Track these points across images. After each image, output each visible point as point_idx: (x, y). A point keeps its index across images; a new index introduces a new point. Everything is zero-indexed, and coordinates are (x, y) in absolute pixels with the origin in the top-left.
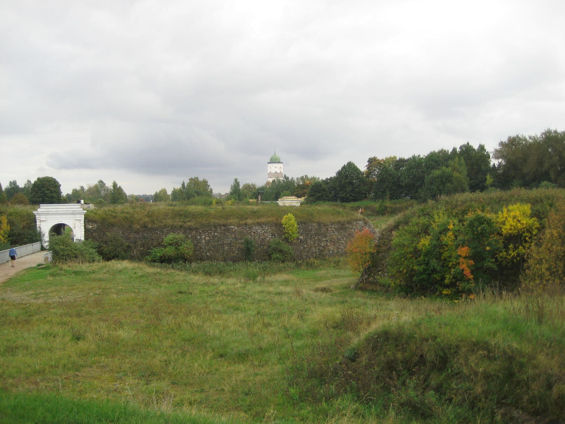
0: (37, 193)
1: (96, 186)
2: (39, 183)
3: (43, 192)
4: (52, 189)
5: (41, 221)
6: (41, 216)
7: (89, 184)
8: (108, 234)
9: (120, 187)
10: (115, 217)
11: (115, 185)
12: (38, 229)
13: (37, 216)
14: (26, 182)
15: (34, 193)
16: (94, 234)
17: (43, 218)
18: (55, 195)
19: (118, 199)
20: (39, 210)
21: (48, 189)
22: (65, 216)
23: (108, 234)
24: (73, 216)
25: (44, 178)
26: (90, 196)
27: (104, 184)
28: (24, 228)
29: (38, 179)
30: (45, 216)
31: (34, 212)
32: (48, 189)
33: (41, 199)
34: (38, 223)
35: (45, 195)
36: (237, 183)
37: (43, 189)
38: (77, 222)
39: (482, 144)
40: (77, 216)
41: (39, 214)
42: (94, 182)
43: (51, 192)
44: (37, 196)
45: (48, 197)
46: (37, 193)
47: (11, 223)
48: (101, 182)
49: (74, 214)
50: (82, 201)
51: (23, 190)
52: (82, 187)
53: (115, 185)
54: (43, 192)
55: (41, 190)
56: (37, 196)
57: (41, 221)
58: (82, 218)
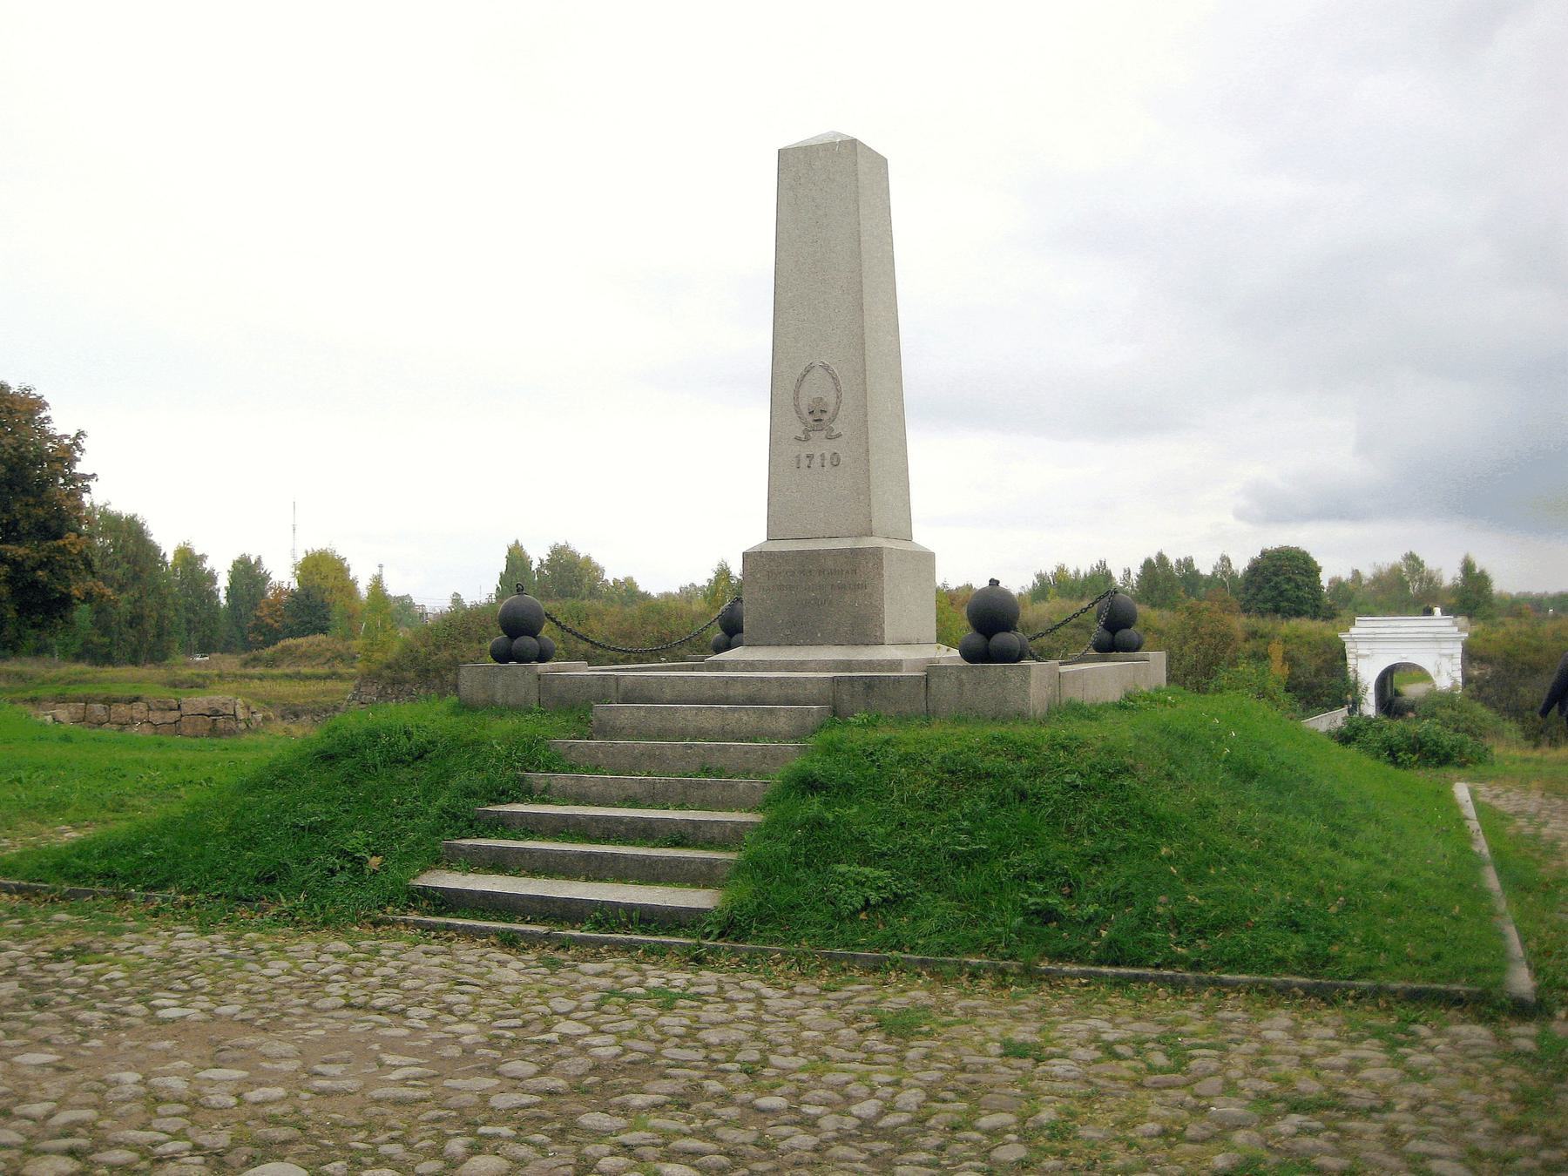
0: (1260, 589)
1: (1395, 570)
2: (1267, 562)
3: (1275, 587)
4: (1299, 578)
5: (1357, 657)
6: (1360, 645)
7: (1379, 563)
8: (1522, 690)
9: (1482, 572)
10: (1538, 650)
11: (1468, 567)
12: (1352, 675)
13: (1347, 646)
14: (1095, 563)
15: (1252, 591)
16: (1487, 690)
17: (1363, 649)
18: (1305, 593)
19: (1478, 604)
20: (1353, 630)
21: (1289, 580)
22: (1399, 646)
23: (1522, 690)
24: (1435, 645)
25: (1278, 551)
26: (1380, 597)
27: (1421, 565)
28: (1318, 672)
29: (1263, 553)
30: (1367, 646)
31: (1343, 636)
32: (1289, 580)
33: (1269, 605)
34: (1351, 661)
35: (1281, 594)
36: (516, 559)
37: (1275, 579)
38: (1445, 661)
39: (807, 126)
40: (1444, 645)
41: (1353, 640)
42: (1390, 557)
43: (1298, 587)
44: (1260, 597)
45: (1288, 600)
46: (1260, 589)
47: (1289, 659)
48: (1411, 558)
49: (1436, 640)
50: (1437, 610)
51: (1210, 581)
52: (1356, 573)
53: (1468, 567)
54: (1275, 587)
55: (1269, 581)
56: (1260, 597)
57: (1357, 657)
58: (1457, 650)
